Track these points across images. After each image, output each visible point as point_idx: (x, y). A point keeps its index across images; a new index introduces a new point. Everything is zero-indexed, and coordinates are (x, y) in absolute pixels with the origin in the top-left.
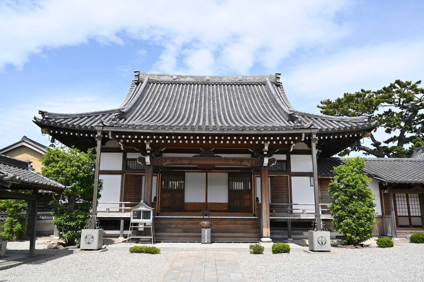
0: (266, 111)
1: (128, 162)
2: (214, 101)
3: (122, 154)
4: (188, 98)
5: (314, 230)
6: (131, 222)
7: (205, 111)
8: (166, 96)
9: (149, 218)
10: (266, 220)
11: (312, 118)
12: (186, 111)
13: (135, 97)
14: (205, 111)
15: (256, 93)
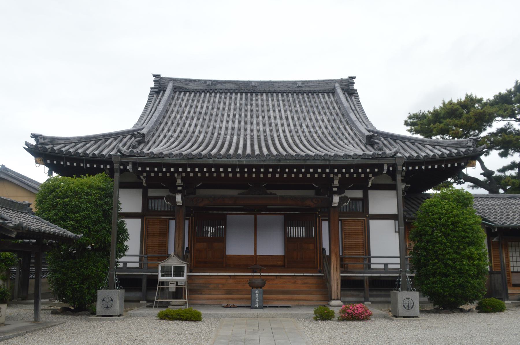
0: (335, 131)
1: (150, 201)
2: (263, 117)
3: (141, 190)
4: (229, 112)
5: (398, 290)
6: (159, 281)
7: (252, 131)
8: (198, 110)
9: (183, 276)
10: (335, 278)
11: (398, 141)
12: (226, 131)
13: (156, 112)
14: (252, 131)
15: (321, 105)
